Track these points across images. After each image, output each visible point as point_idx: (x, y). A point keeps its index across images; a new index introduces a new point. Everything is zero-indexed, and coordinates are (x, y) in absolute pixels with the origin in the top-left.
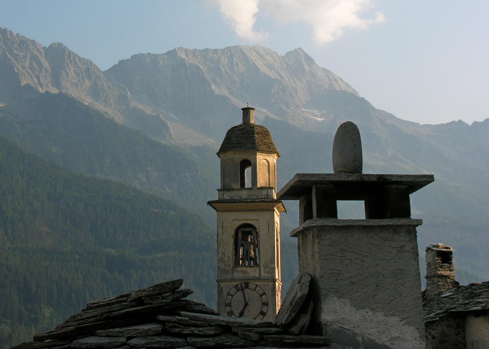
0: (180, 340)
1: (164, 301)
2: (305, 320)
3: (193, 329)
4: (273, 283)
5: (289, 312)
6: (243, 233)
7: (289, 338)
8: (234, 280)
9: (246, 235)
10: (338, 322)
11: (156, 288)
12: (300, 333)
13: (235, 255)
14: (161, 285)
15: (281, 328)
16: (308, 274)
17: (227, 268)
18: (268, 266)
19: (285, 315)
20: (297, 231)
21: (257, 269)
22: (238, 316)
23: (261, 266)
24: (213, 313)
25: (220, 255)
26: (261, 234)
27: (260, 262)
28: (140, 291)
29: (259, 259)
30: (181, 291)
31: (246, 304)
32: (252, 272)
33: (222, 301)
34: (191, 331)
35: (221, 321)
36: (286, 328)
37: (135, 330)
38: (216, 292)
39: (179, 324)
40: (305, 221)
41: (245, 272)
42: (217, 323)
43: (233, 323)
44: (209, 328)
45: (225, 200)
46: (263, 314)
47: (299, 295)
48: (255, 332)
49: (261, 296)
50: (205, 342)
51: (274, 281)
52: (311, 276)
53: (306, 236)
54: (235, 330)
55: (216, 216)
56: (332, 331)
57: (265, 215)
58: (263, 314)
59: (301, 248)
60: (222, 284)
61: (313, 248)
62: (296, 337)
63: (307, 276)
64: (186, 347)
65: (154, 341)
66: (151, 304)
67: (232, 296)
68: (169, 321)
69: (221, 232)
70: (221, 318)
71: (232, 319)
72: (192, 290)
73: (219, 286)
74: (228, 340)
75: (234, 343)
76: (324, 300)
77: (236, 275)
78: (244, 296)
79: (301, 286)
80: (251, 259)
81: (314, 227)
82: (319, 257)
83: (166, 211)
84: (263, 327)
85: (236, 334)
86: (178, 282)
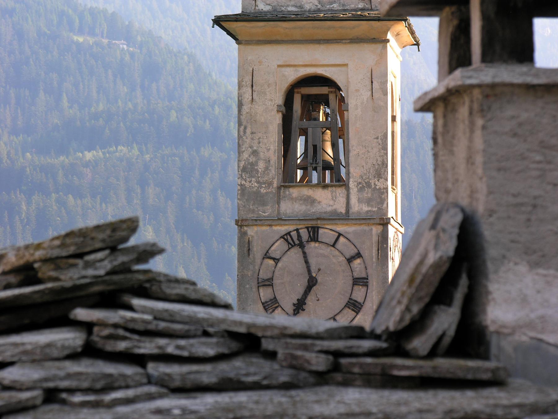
0: (129, 370)
1: (91, 272)
2: (446, 321)
3: (162, 342)
4: (380, 228)
5: (405, 301)
6: (306, 99)
7: (403, 367)
8: (280, 220)
9: (313, 103)
10: (530, 325)
11: (68, 241)
12: (433, 354)
13: (285, 156)
14: (83, 234)
15: (386, 341)
16: (456, 205)
17: (263, 191)
18: (368, 185)
19: (394, 308)
20: (429, 97)
21: (340, 192)
22: (291, 311)
23: (352, 184)
24: (227, 307)
25: (245, 155)
26: (352, 102)
27: (348, 173)
28: (27, 247)
29: (347, 166)
30: (133, 248)
31: (312, 283)
32: (328, 200)
33: (250, 274)
34: (160, 348)
35: (235, 323)
36: (397, 341)
37: (16, 345)
38: (234, 250)
39: (126, 329)
40: (451, 70)
41: (311, 201)
42: (224, 327)
43: (266, 328)
44: (204, 340)
45: (261, 12)
46: (355, 306)
47: (432, 258)
48: (321, 352)
49: (350, 260)
50: (192, 376)
51: (385, 223)
52: (463, 210)
53: (454, 110)
54: (267, 345)
55: (236, 53)
56: (516, 349)
57: (365, 54)
58: (355, 306)
59: (440, 140)
60: (251, 231)
61: (471, 140)
62: (421, 363)
63: (453, 211)
64: (353, 397)
65: (62, 373)
66: (57, 279)
67: (277, 260)
68: (103, 324)
69: (247, 96)
70: (235, 315)
71: (280, 319)
72: (161, 245)
73: (242, 235)
74: (252, 370)
75: (265, 378)
76: (496, 272)
77: (288, 208)
78: (307, 262)
79: (438, 237)
80: (327, 166)
81: (472, 86)
82: (485, 163)
83: (105, 41)
84: (340, 338)
85: (271, 355)
86: (124, 226)
